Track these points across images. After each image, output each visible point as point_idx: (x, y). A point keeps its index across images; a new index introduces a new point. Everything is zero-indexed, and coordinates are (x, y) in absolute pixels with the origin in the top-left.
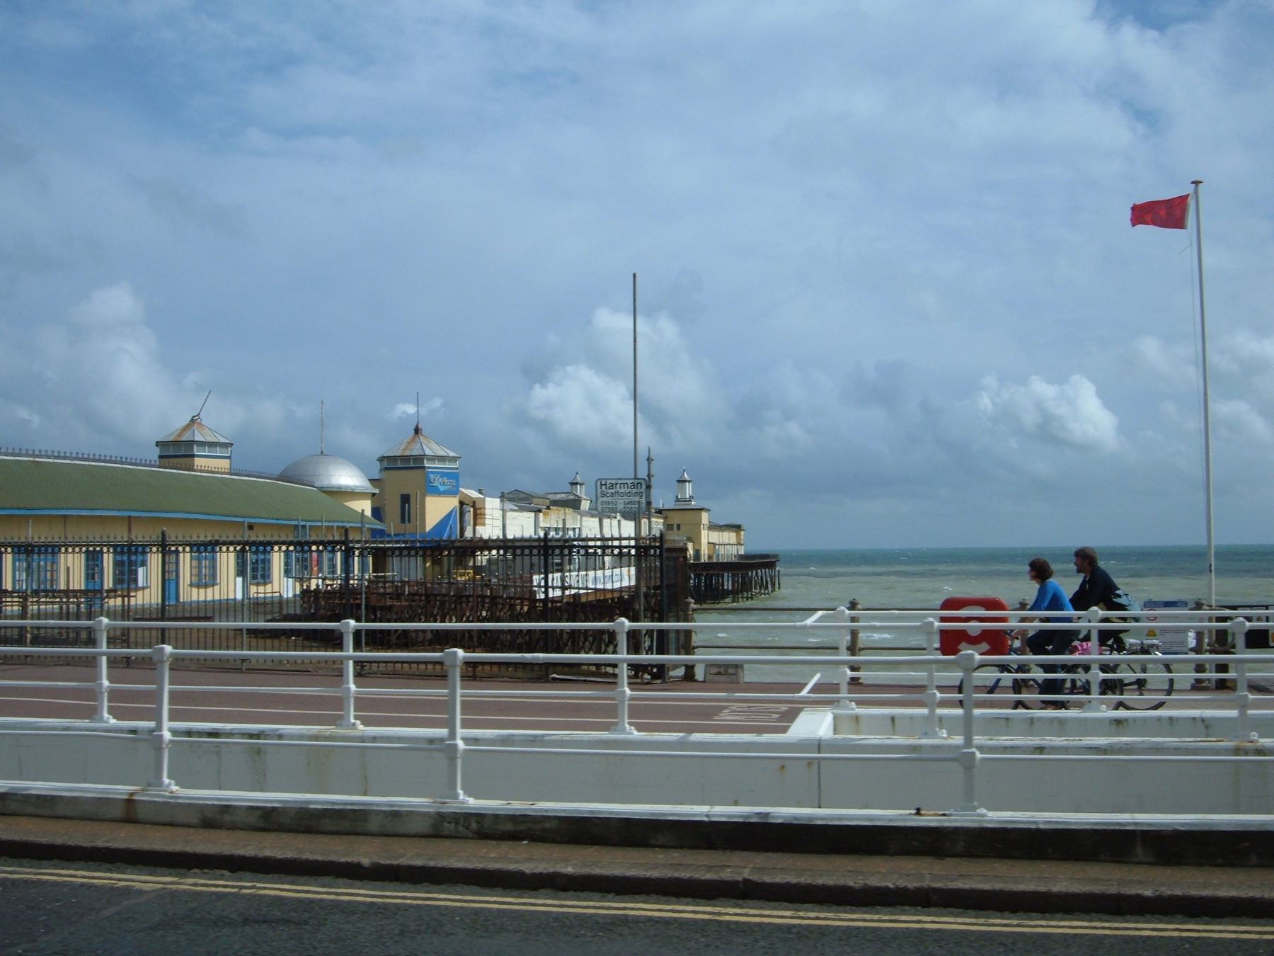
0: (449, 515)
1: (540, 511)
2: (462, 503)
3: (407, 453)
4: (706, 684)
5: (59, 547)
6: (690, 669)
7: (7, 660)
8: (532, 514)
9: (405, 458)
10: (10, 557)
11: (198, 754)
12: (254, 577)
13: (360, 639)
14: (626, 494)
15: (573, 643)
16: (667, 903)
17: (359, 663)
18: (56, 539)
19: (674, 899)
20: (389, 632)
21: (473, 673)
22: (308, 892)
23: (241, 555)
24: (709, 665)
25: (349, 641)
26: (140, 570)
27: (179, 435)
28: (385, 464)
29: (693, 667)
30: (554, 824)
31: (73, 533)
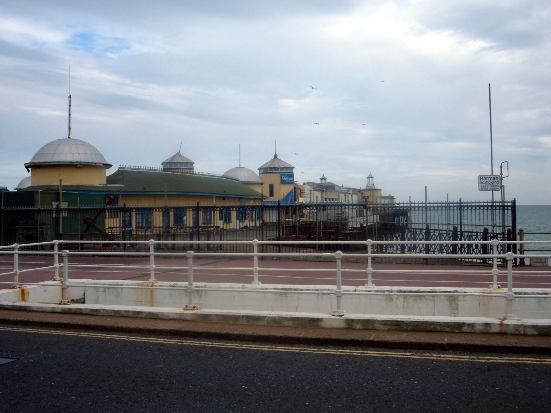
0: (290, 192)
1: (323, 191)
2: (295, 188)
3: (272, 166)
4: (531, 266)
5: (62, 210)
6: (522, 260)
7: (2, 255)
8: (320, 192)
9: (271, 169)
10: (235, 212)
11: (484, 304)
12: (225, 220)
14: (491, 182)
15: (468, 250)
16: (455, 354)
17: (373, 259)
18: (152, 206)
19: (192, 338)
20: (77, 244)
21: (345, 261)
22: (517, 360)
23: (221, 212)
24: (531, 259)
25: (370, 249)
26: (185, 218)
27: (173, 159)
28: (262, 171)
29: (524, 259)
30: (417, 323)
31: (161, 203)
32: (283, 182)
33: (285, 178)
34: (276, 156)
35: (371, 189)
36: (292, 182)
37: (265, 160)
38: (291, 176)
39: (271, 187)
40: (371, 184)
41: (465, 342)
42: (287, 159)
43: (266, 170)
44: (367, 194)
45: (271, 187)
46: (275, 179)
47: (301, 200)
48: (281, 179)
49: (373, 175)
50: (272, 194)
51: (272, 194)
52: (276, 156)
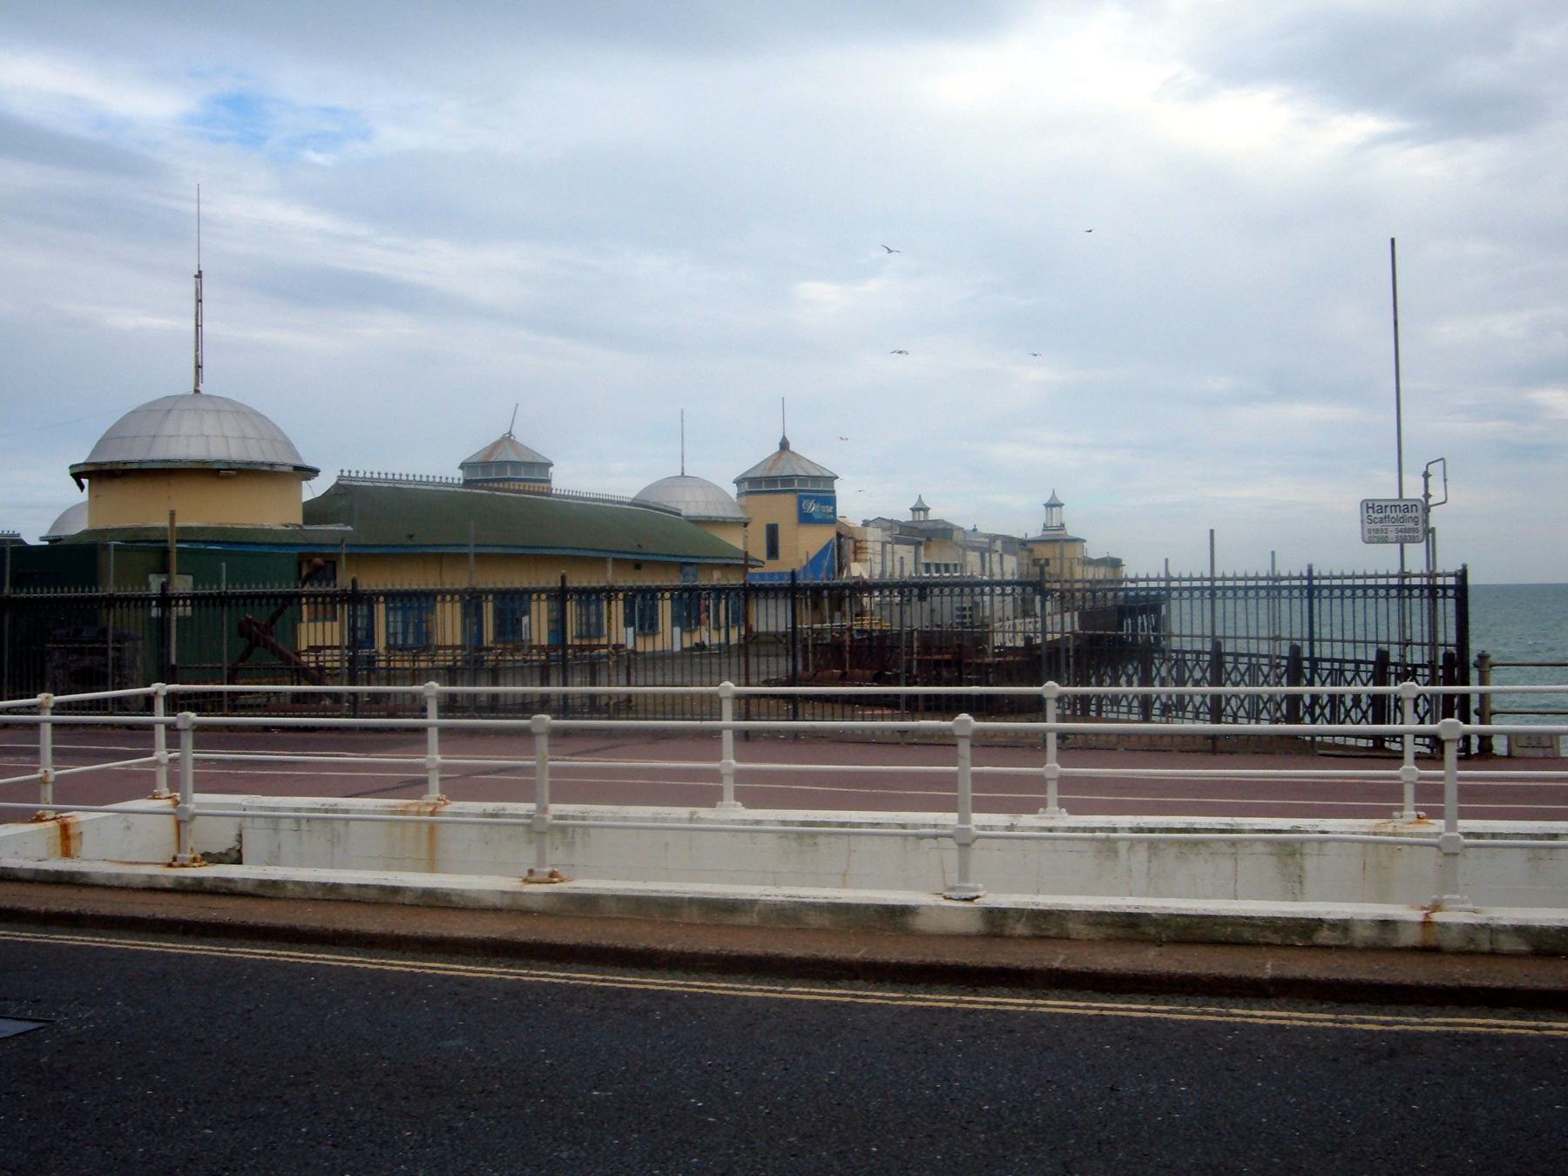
0: (826, 548)
1: (920, 543)
2: (839, 536)
3: (773, 473)
4: (1510, 759)
5: (177, 599)
6: (1485, 739)
7: (6, 726)
8: (912, 548)
9: (771, 480)
10: (668, 604)
11: (1376, 865)
12: (642, 627)
13: (450, 706)
15: (1332, 713)
16: (1296, 1009)
17: (1062, 736)
18: (431, 587)
19: (547, 964)
20: (220, 693)
21: (983, 744)
23: (629, 604)
24: (1511, 737)
25: (1052, 709)
26: (525, 620)
27: (491, 454)
28: (746, 487)
29: (1490, 737)
30: (1187, 921)
31: (458, 579)
32: (805, 518)
33: (812, 508)
34: (784, 445)
35: (1057, 539)
36: (831, 519)
37: (754, 454)
38: (830, 500)
39: (772, 531)
40: (1055, 523)
41: (1323, 975)
42: (816, 453)
43: (756, 484)
44: (1044, 552)
45: (772, 531)
46: (782, 509)
47: (857, 570)
48: (800, 509)
49: (1061, 499)
50: (773, 551)
51: (773, 551)
52: (784, 445)
